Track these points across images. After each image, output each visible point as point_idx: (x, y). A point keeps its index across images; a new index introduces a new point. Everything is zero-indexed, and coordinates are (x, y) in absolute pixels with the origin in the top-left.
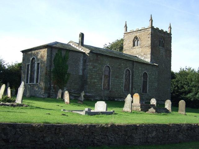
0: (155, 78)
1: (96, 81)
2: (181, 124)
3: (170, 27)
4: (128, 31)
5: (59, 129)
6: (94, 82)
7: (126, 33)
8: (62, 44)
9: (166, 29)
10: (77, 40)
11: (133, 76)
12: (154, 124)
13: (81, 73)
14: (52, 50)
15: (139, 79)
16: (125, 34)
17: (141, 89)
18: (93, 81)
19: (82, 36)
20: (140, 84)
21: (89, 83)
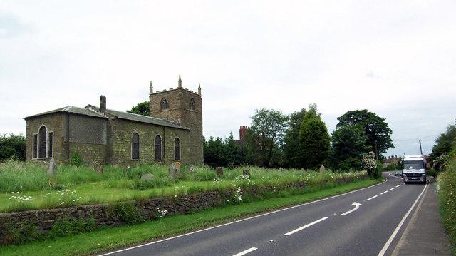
3: (200, 89)
4: (154, 92)
7: (152, 95)
8: (78, 109)
9: (195, 90)
10: (97, 104)
11: (164, 142)
13: (105, 143)
14: (68, 121)
16: (42, 154)
19: (103, 99)
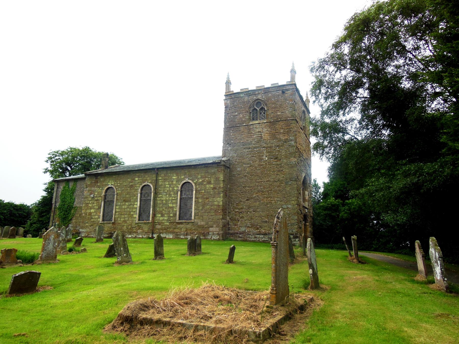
0: (214, 188)
1: (92, 211)
2: (168, 244)
5: (376, 61)
6: (90, 214)
12: (62, 154)
15: (173, 196)
17: (176, 214)
18: (88, 211)
20: (174, 205)
21: (84, 215)
